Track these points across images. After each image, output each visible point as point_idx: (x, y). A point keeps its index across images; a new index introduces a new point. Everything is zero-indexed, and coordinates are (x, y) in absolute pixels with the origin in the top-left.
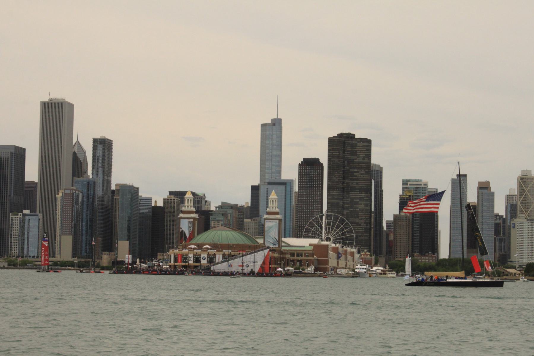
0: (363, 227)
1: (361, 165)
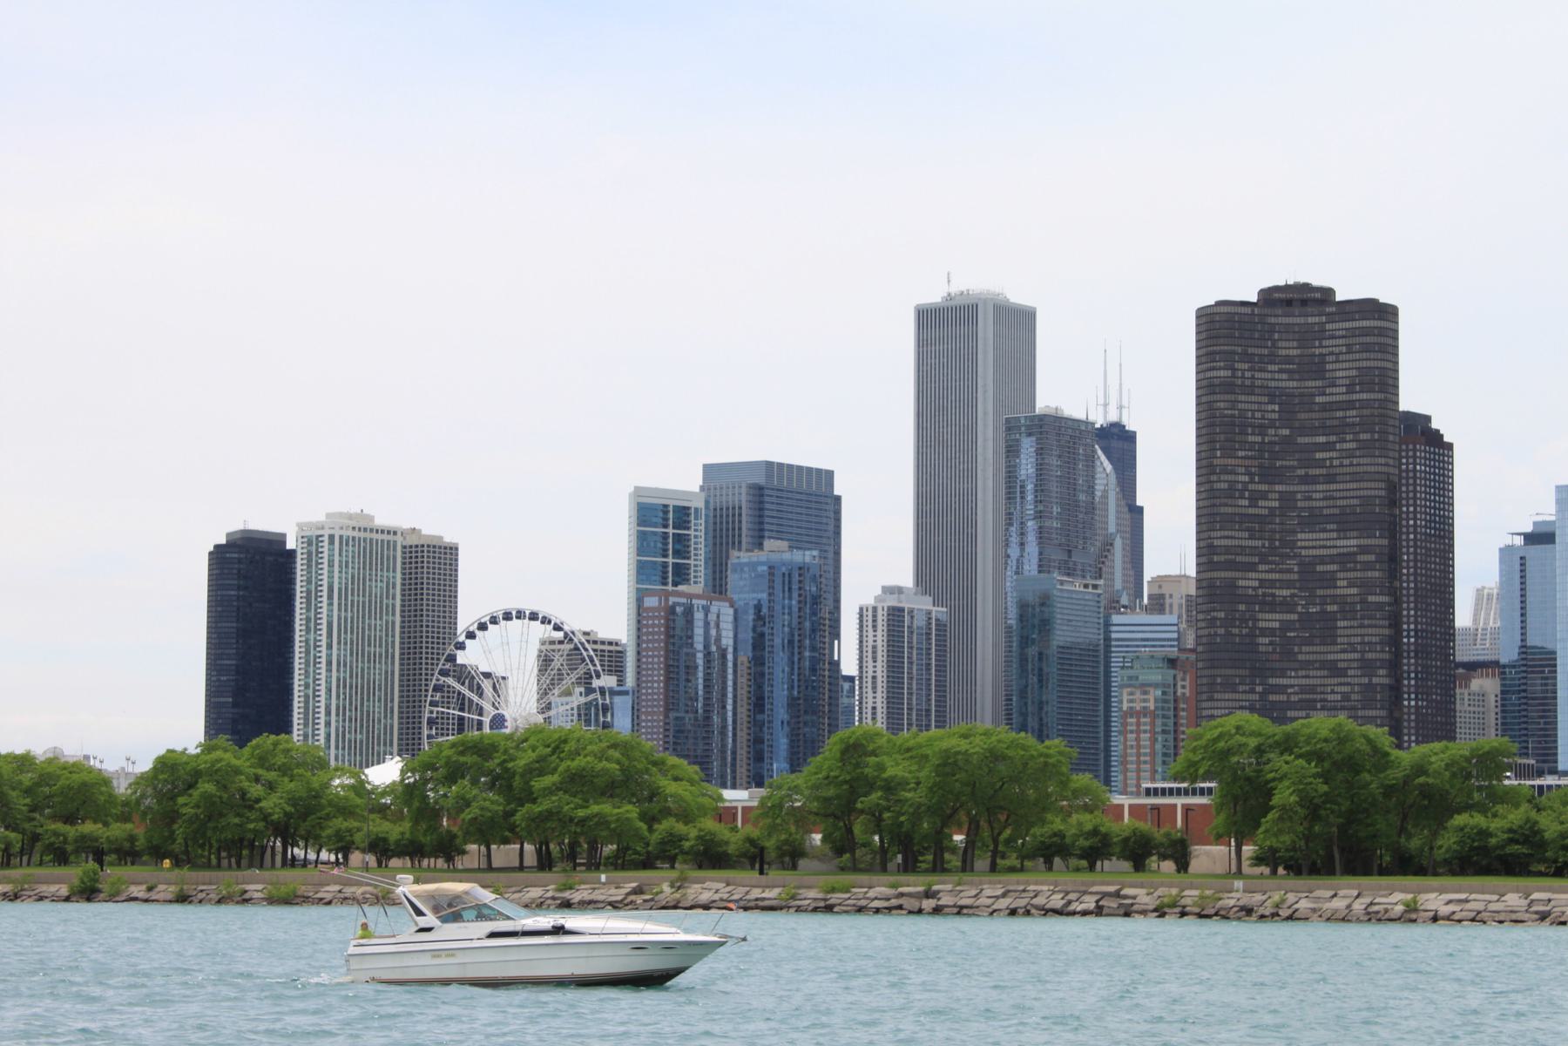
0: (1356, 680)
1: (1340, 414)
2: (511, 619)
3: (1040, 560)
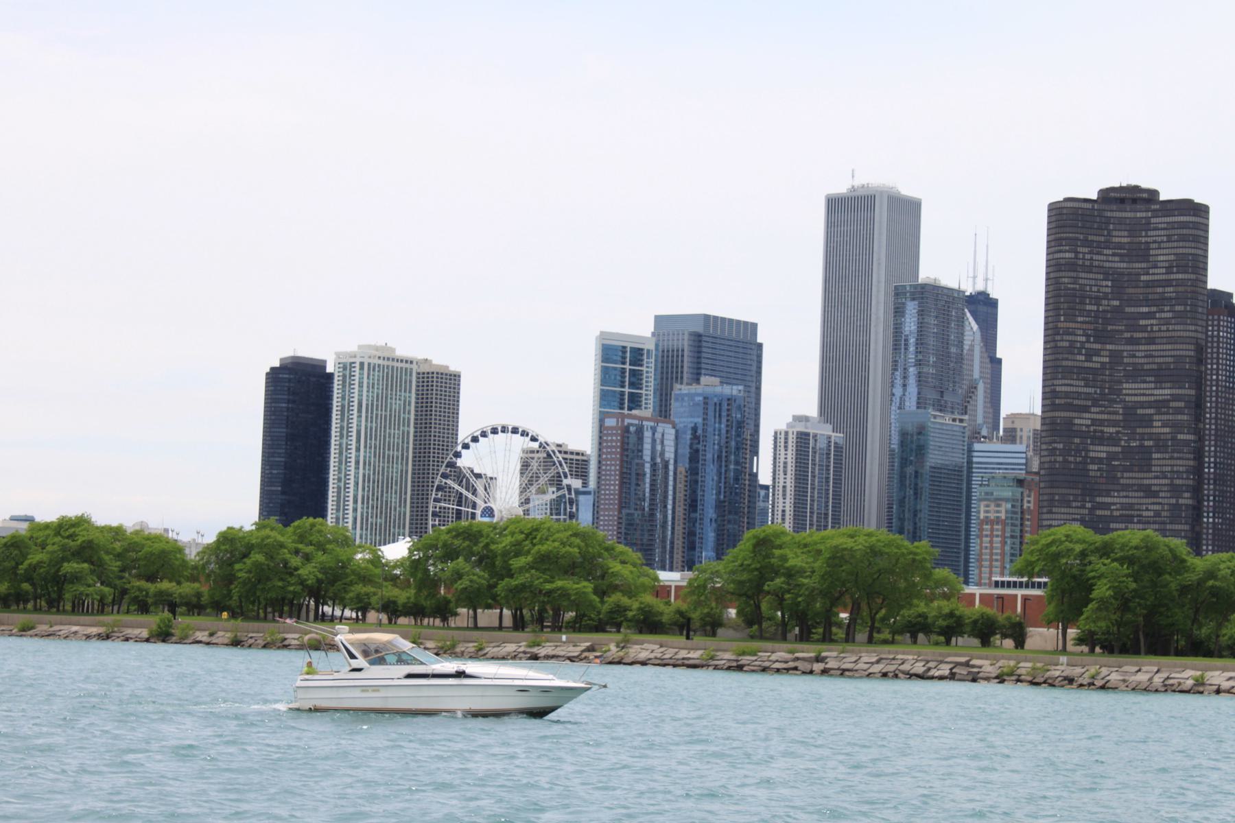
0: (1166, 501)
1: (1160, 290)
2: (497, 433)
3: (918, 398)
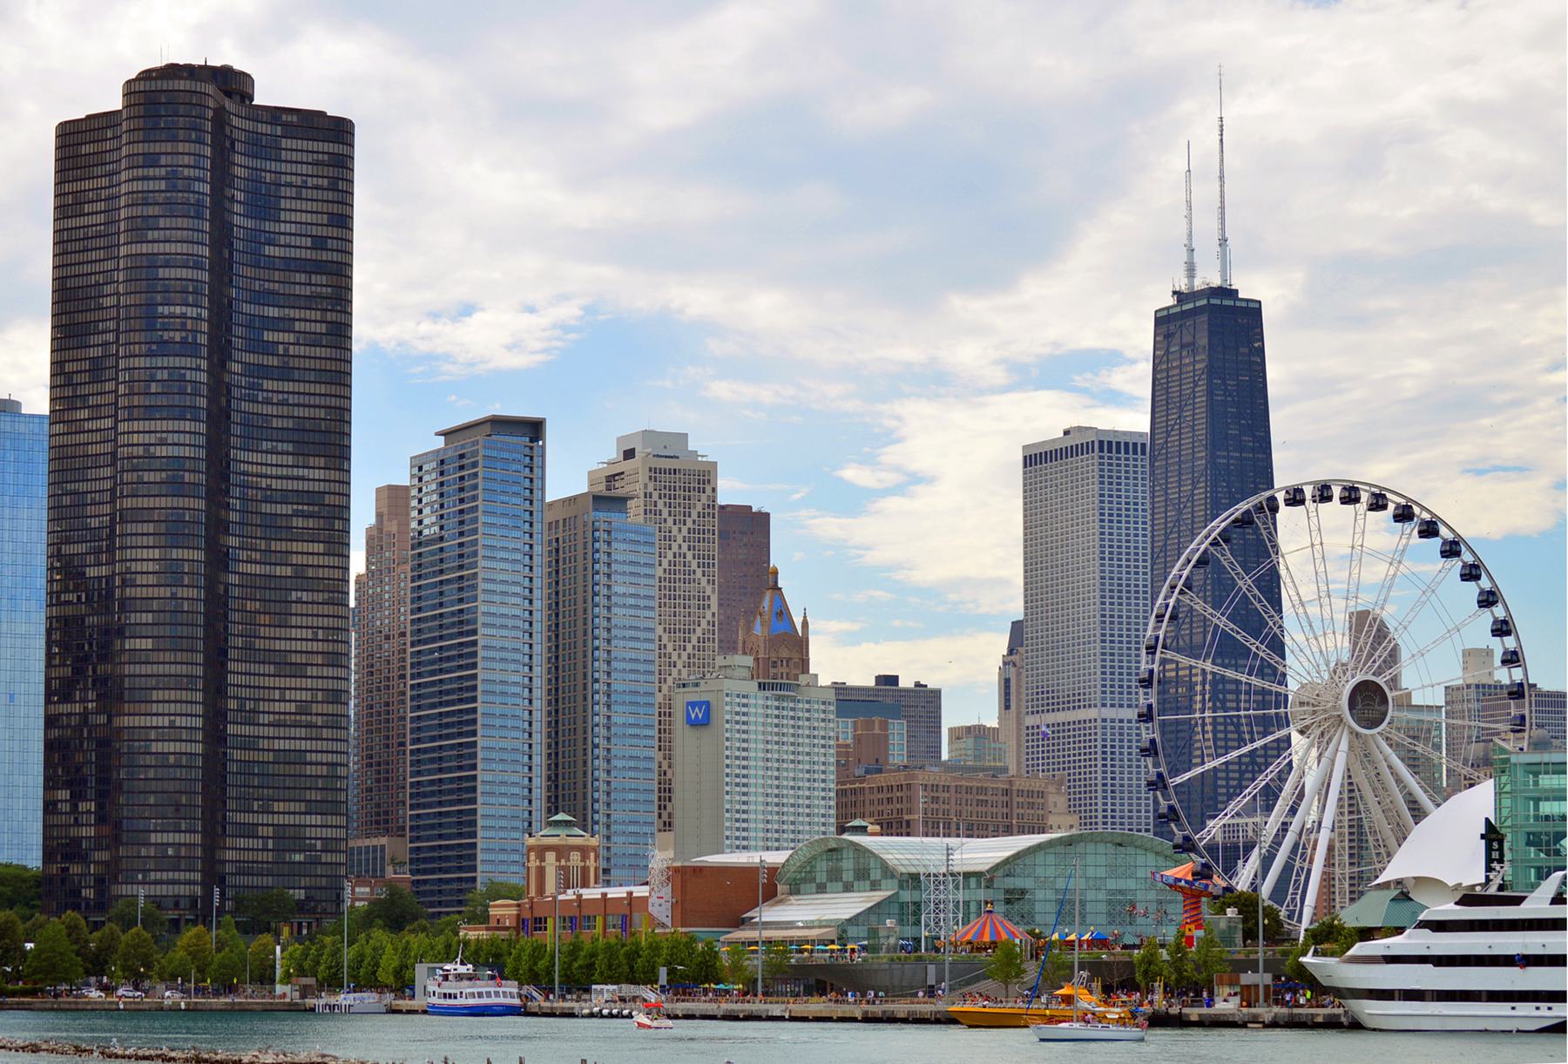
2: (1302, 502)
